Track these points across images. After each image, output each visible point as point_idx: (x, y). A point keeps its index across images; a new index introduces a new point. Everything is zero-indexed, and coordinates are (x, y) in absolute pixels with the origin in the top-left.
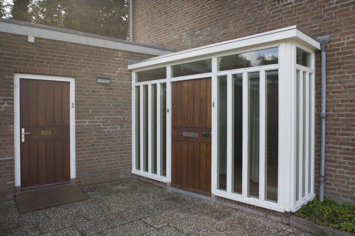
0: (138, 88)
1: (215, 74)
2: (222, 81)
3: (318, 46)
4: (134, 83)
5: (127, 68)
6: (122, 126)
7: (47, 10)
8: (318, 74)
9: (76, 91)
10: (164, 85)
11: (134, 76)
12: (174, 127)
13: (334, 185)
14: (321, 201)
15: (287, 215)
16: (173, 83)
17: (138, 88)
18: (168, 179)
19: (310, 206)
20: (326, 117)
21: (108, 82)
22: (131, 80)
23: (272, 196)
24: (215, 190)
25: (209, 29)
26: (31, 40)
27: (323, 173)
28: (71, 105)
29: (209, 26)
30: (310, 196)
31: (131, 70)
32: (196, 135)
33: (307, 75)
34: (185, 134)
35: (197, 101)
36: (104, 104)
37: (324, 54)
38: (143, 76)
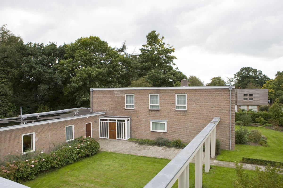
0: (101, 122)
1: (117, 122)
2: (118, 123)
7: (30, 81)
8: (130, 122)
10: (107, 123)
11: (100, 120)
13: (138, 76)
15: (126, 140)
17: (101, 122)
18: (108, 138)
19: (20, 182)
24: (117, 138)
26: (88, 117)
30: (130, 138)
36: (29, 108)
38: (101, 120)
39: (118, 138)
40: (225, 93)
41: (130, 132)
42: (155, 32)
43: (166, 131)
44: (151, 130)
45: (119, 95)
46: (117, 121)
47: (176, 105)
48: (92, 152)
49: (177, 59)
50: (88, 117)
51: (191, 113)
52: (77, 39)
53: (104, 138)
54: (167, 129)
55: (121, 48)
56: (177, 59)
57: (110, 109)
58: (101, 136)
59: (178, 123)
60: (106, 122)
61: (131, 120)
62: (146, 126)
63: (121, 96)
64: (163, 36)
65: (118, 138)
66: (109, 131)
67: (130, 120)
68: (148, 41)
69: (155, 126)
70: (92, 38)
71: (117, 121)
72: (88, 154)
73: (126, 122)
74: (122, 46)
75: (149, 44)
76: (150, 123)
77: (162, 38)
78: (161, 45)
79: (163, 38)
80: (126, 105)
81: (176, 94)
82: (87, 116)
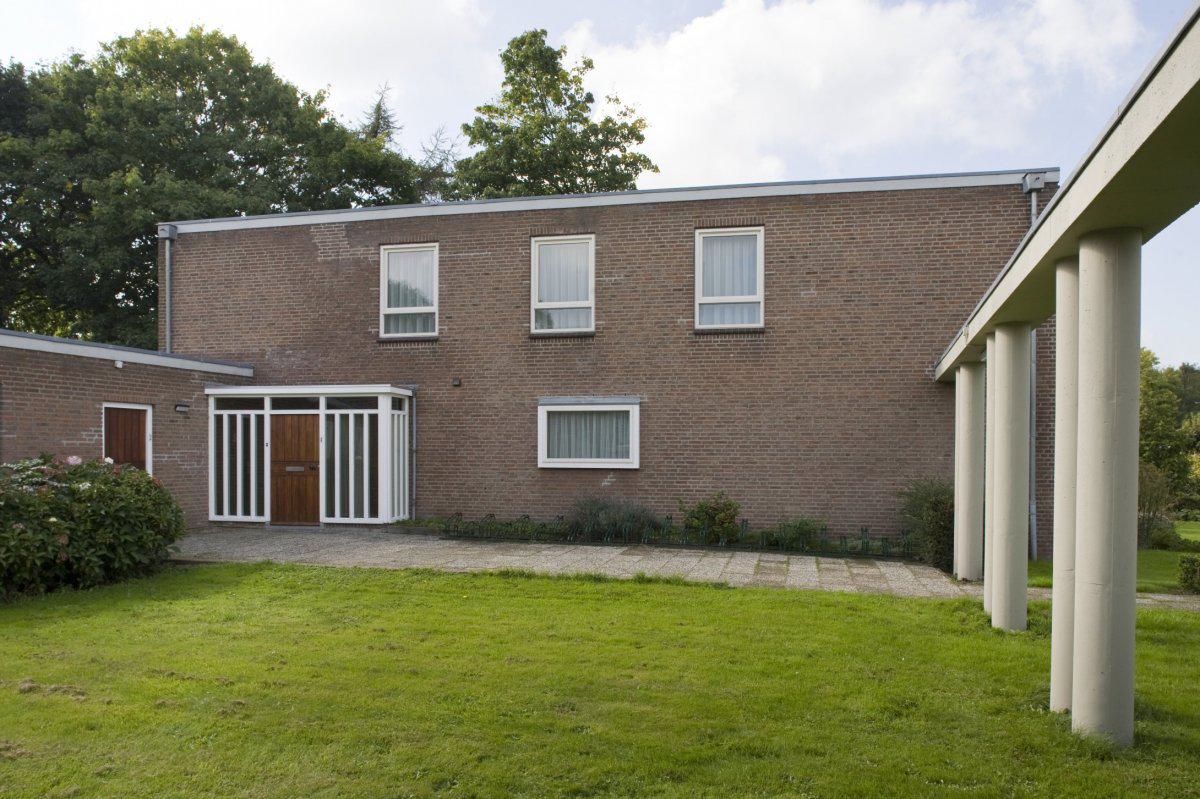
0: (219, 419)
1: (322, 411)
2: (330, 418)
3: (410, 393)
4: (212, 411)
5: (203, 391)
6: (199, 462)
8: (411, 416)
9: (154, 420)
10: (260, 419)
11: (212, 402)
12: (273, 462)
14: (179, 227)
15: (385, 525)
16: (272, 416)
17: (219, 419)
18: (267, 517)
20: (417, 452)
21: (186, 409)
22: (207, 407)
23: (374, 512)
24: (323, 518)
25: (304, 352)
26: (119, 365)
27: (414, 497)
28: (324, 440)
29: (305, 349)
31: (208, 395)
32: (302, 469)
33: (401, 418)
34: (289, 469)
35: (303, 436)
37: (414, 400)
38: (223, 403)
39: (331, 513)
40: (997, 213)
41: (411, 480)
42: (544, 38)
43: (633, 461)
44: (543, 461)
45: (344, 256)
46: (329, 406)
47: (699, 298)
48: (112, 548)
49: (656, 169)
50: (119, 365)
51: (793, 342)
52: (110, 38)
53: (240, 517)
54: (641, 448)
55: (367, 122)
56: (656, 169)
57: (283, 347)
58: (220, 511)
59: (712, 408)
60: (253, 413)
61: (415, 407)
62: (508, 437)
63: (357, 262)
64: (590, 56)
65: (331, 513)
66: (272, 472)
67: (411, 406)
68: (511, 80)
69: (564, 436)
70: (196, 41)
71: (323, 403)
72: (79, 559)
73: (384, 409)
74: (371, 111)
75: (515, 98)
76: (534, 421)
77: (581, 65)
78: (575, 104)
79: (589, 64)
80: (387, 317)
81: (698, 232)
82: (120, 356)
